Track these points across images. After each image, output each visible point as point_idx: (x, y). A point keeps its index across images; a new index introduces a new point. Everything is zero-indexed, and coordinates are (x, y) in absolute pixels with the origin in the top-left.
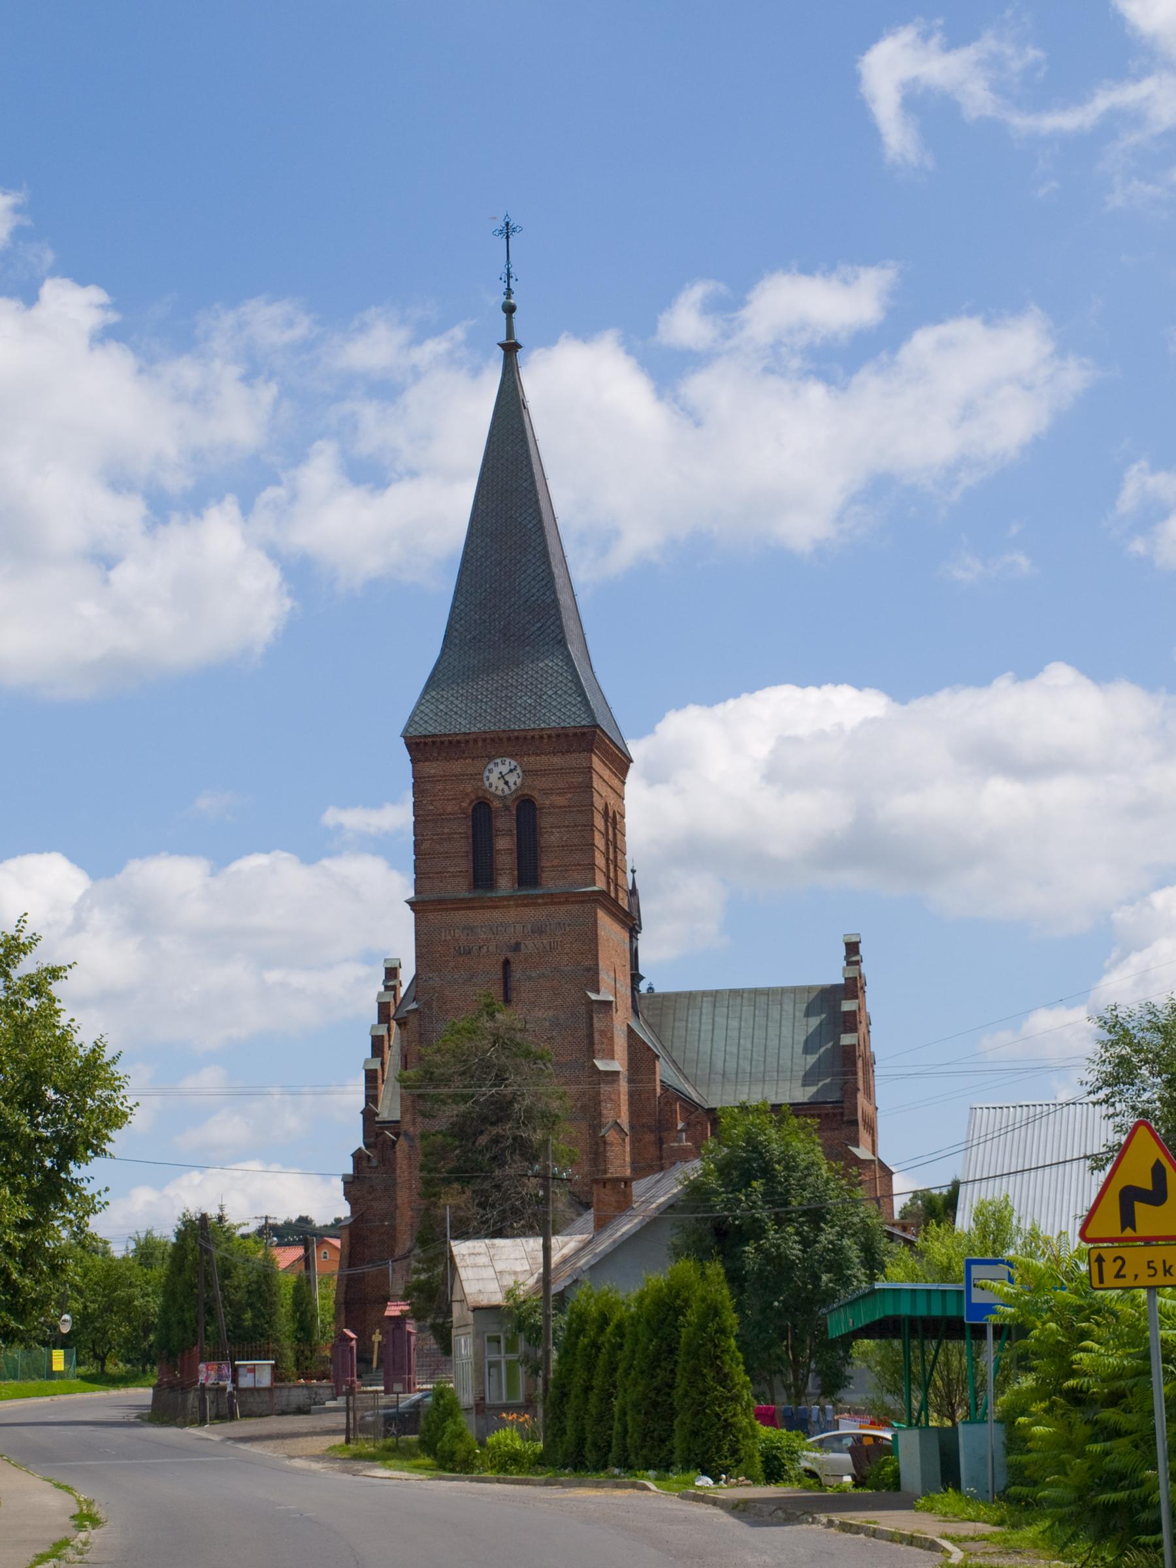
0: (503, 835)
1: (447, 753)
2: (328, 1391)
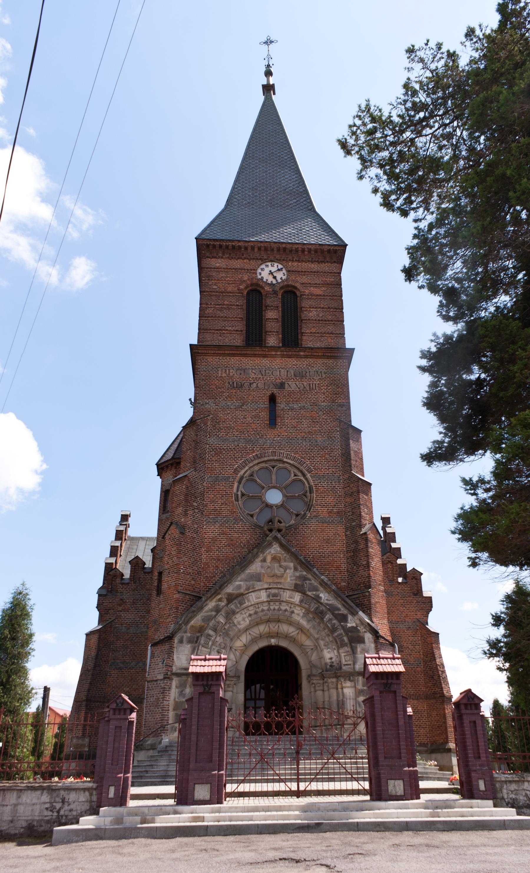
0: (272, 309)
1: (230, 254)
2: (83, 797)
